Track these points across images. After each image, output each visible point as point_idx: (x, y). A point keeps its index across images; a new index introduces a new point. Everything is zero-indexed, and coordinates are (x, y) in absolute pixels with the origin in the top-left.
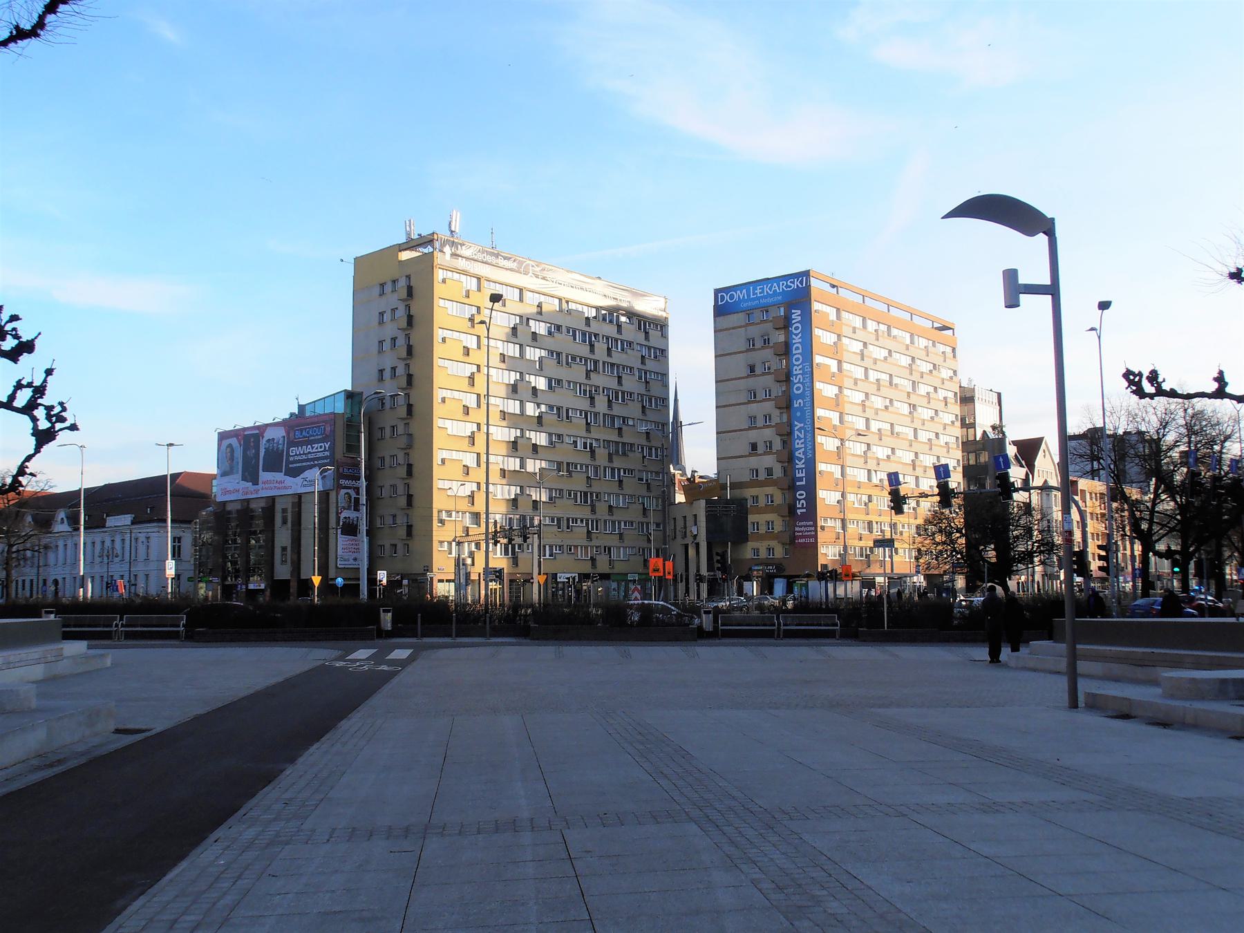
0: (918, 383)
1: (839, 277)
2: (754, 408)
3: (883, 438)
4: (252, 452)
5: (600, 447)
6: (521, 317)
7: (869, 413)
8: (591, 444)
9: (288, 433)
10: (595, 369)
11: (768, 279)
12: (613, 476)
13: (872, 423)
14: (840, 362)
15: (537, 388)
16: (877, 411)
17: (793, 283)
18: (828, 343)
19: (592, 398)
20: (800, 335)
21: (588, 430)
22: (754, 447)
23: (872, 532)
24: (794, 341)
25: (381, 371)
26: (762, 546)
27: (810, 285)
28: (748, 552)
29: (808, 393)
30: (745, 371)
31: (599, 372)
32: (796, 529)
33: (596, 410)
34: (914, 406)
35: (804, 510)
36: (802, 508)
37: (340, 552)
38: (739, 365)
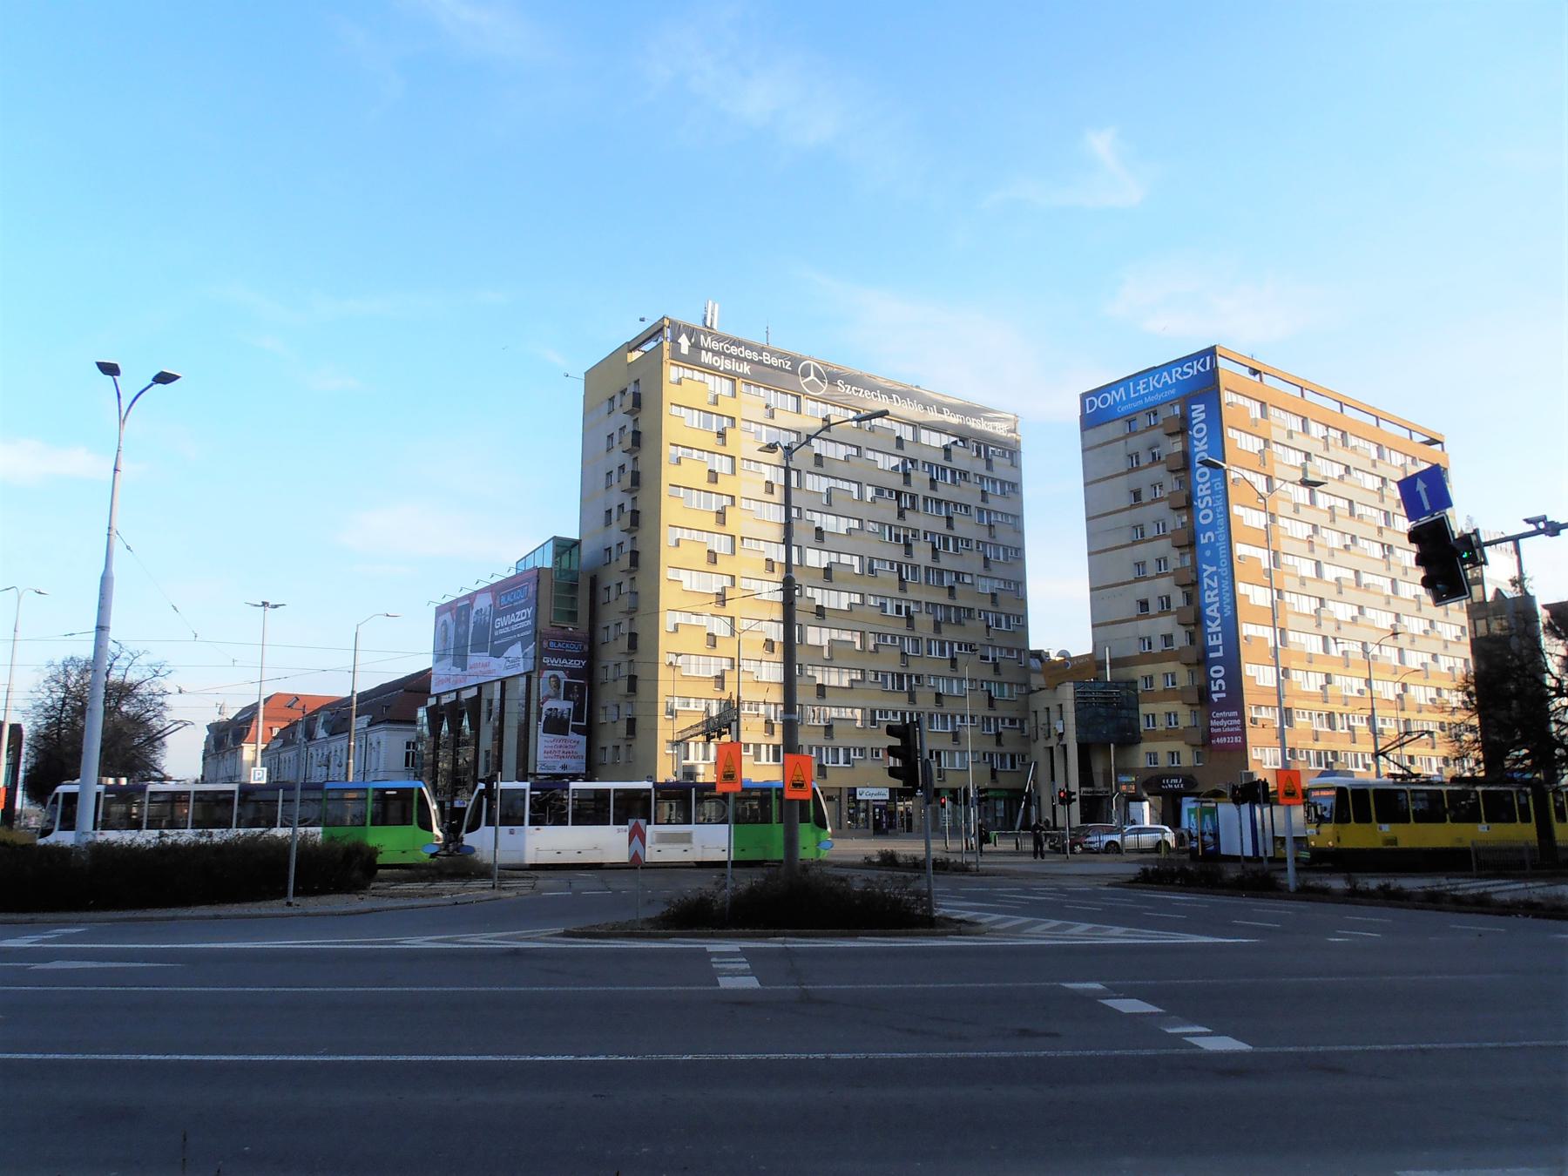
0: (1394, 514)
1: (1263, 359)
2: (1141, 552)
3: (1344, 590)
4: (461, 630)
5: (921, 612)
6: (798, 433)
7: (1320, 554)
8: (908, 608)
9: (494, 599)
10: (913, 507)
11: (1155, 368)
12: (942, 651)
13: (1326, 568)
14: (1269, 479)
15: (824, 529)
16: (1332, 552)
17: (1192, 367)
18: (1250, 450)
19: (908, 546)
20: (1205, 439)
21: (903, 588)
22: (1144, 605)
23: (1334, 729)
24: (1196, 450)
25: (609, 512)
26: (1162, 748)
27: (1217, 367)
28: (1141, 757)
29: (1221, 522)
30: (1127, 500)
31: (918, 511)
32: (1213, 723)
33: (915, 561)
34: (1390, 547)
35: (1224, 695)
36: (1220, 691)
37: (540, 757)
38: (1118, 495)
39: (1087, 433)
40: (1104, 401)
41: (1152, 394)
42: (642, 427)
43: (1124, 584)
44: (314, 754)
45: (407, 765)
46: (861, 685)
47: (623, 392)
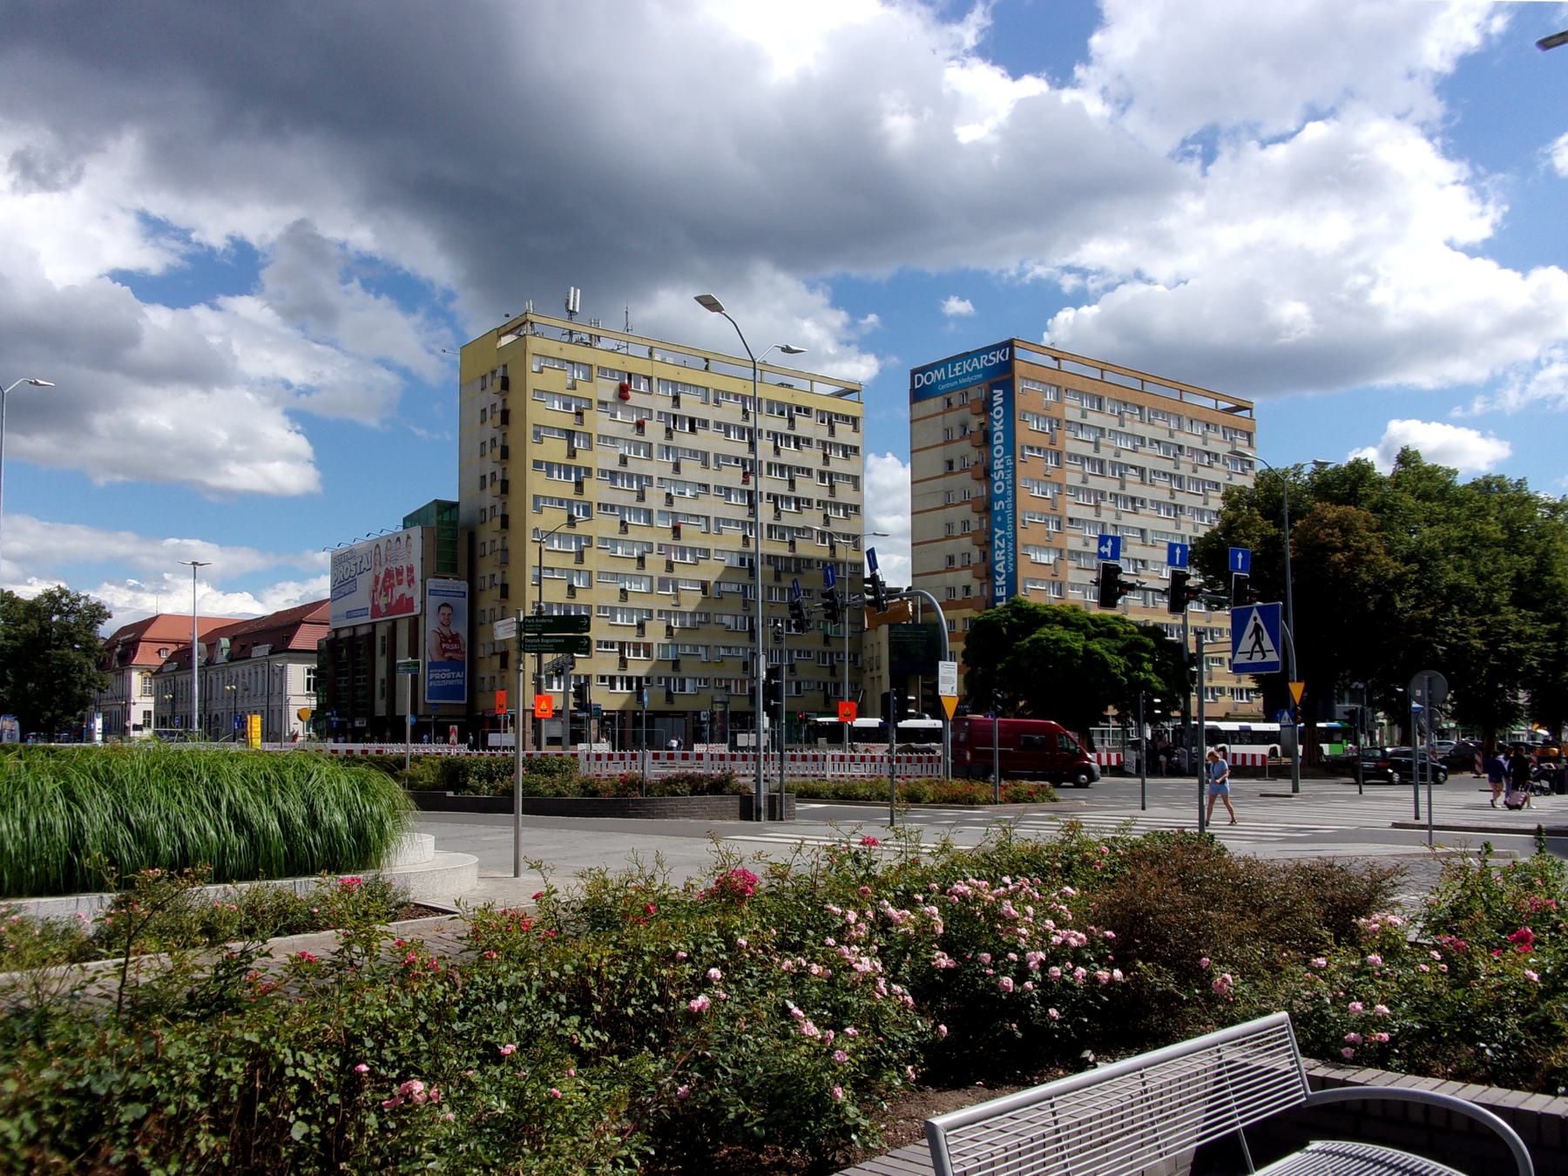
17: (994, 356)
22: (951, 559)
25: (483, 478)
29: (1010, 492)
38: (934, 461)
39: (916, 406)
40: (929, 378)
41: (963, 376)
42: (510, 405)
43: (936, 541)
44: (214, 677)
45: (308, 689)
46: (706, 627)
47: (493, 372)
